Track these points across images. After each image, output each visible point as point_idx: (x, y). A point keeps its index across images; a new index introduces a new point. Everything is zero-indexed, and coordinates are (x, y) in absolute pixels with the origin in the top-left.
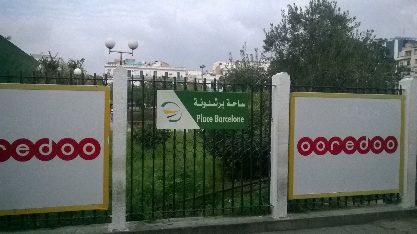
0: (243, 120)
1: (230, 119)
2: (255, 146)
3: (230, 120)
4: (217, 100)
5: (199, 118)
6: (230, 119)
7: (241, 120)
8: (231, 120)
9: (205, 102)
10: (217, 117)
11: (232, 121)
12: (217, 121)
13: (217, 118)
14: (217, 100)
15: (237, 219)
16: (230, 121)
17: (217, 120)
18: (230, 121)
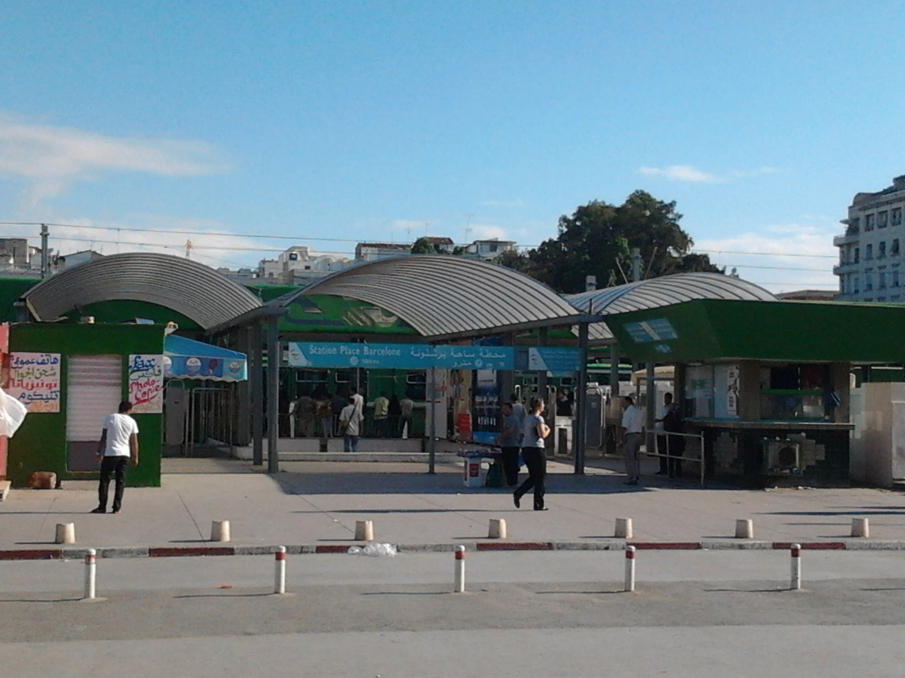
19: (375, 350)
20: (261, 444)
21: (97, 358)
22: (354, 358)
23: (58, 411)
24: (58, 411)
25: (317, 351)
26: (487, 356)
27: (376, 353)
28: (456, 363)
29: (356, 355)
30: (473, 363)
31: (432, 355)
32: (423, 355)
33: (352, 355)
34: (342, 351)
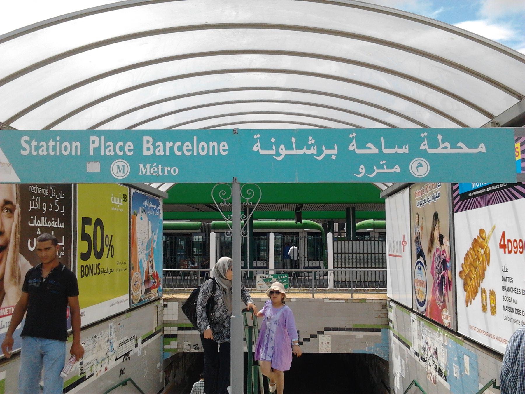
0: (226, 147)
1: (190, 148)
2: (303, 221)
3: (188, 151)
4: (313, 141)
5: (96, 145)
6: (190, 148)
7: (221, 148)
8: (192, 150)
9: (282, 146)
10: (148, 141)
11: (195, 153)
12: (151, 152)
13: (150, 145)
14: (313, 141)
15: (7, 327)
16: (191, 153)
17: (148, 149)
18: (191, 153)
19: (168, 145)
20: (251, 368)
21: (473, 344)
22: (121, 163)
23: (271, 140)
24: (271, 140)
25: (37, 148)
26: (439, 150)
27: (171, 149)
28: (362, 169)
29: (125, 157)
30: (405, 168)
31: (305, 151)
32: (284, 152)
33: (116, 157)
34: (92, 146)
